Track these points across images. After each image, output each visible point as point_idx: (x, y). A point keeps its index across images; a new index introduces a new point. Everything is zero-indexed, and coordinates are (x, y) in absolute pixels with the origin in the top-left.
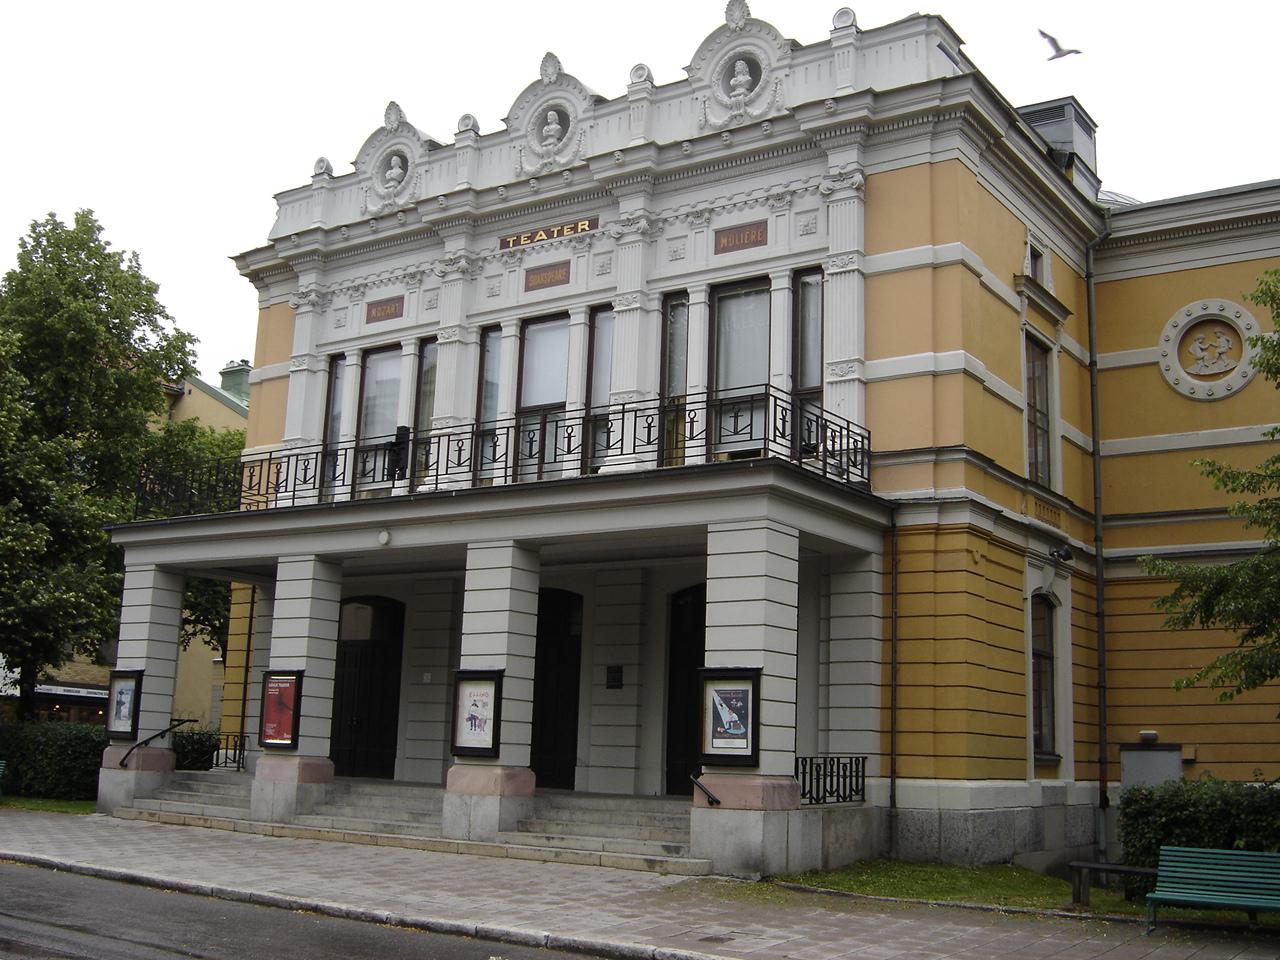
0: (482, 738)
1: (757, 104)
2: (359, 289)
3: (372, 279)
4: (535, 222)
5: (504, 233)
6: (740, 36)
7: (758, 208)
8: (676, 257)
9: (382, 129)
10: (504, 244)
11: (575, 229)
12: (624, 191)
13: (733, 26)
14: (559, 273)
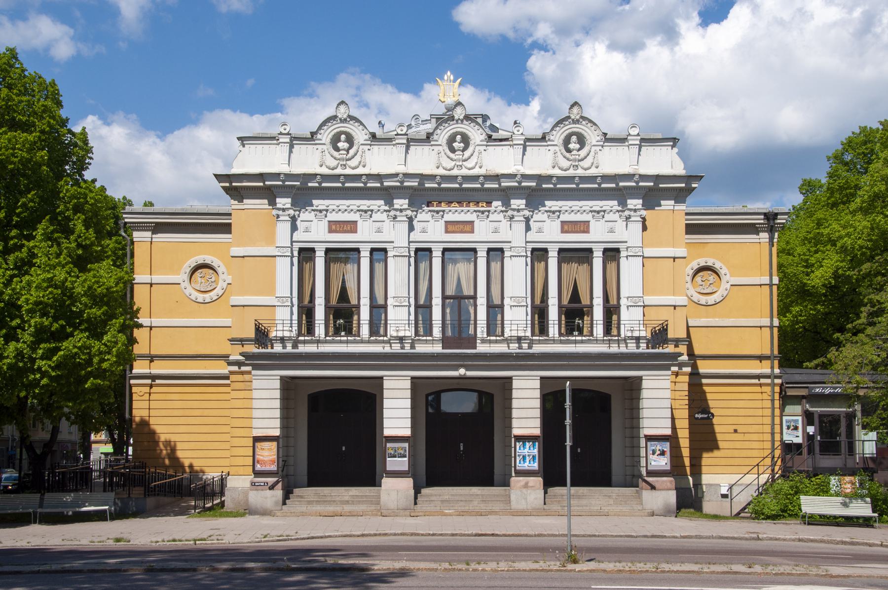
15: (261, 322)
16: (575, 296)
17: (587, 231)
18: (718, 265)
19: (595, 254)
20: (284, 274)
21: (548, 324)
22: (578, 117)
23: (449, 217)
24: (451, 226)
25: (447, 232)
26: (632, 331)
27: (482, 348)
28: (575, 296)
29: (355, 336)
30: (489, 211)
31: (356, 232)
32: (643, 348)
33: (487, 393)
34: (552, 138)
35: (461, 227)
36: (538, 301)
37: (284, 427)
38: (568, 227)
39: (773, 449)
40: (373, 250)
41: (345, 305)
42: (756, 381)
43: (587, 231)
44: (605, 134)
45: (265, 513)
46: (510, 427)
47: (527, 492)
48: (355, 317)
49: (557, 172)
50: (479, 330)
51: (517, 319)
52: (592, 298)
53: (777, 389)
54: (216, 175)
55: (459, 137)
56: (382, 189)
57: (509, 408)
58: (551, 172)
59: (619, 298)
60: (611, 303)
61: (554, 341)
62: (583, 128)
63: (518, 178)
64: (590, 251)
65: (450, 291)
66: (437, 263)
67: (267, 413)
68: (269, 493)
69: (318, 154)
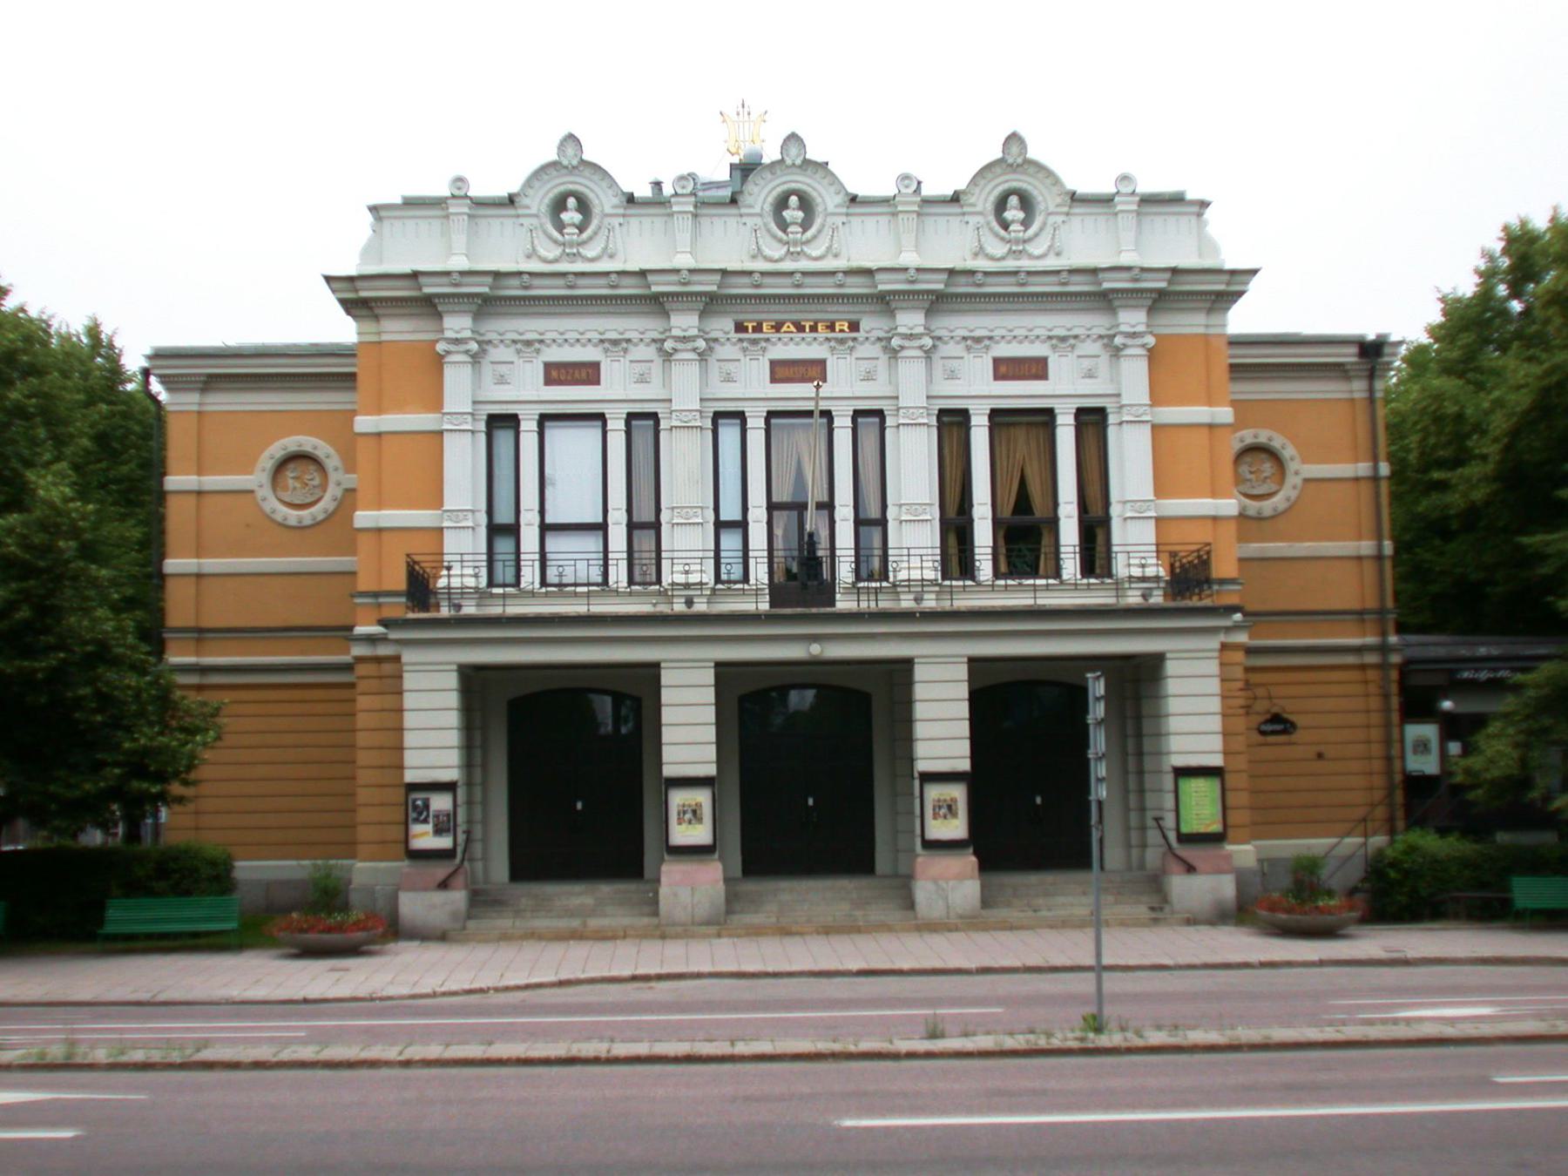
0: (1192, 787)
1: (592, 244)
2: (528, 345)
3: (549, 336)
4: (788, 314)
5: (741, 317)
6: (1014, 172)
7: (590, 348)
8: (501, 380)
9: (554, 164)
10: (740, 328)
11: (831, 327)
12: (450, 308)
13: (565, 162)
14: (814, 371)
15: (417, 558)
16: (1023, 503)
18: (1278, 442)
22: (575, 162)
24: (782, 371)
25: (774, 380)
26: (1143, 566)
27: (844, 603)
28: (1023, 503)
30: (855, 339)
31: (598, 383)
32: (1157, 599)
33: (630, 697)
34: (526, 201)
35: (802, 370)
36: (952, 513)
37: (468, 765)
39: (1390, 789)
40: (631, 417)
41: (1026, 518)
42: (1350, 659)
44: (1074, 194)
46: (911, 760)
47: (951, 883)
48: (1046, 540)
49: (982, 264)
51: (915, 544)
53: (1394, 675)
54: (328, 279)
55: (794, 200)
56: (648, 297)
57: (908, 721)
58: (971, 264)
59: (1107, 504)
60: (1092, 514)
64: (1049, 413)
65: (782, 495)
66: (529, 442)
68: (439, 897)
69: (970, 232)
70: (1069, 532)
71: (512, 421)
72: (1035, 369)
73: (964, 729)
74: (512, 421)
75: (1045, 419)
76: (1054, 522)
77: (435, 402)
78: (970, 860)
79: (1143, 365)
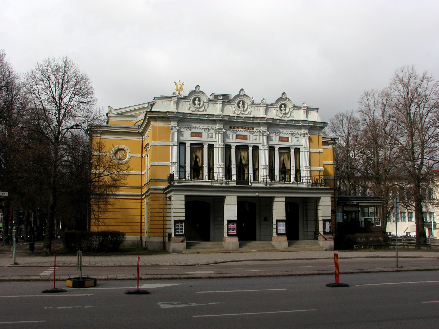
5: (231, 125)
14: (245, 137)
17: (288, 141)
19: (275, 149)
20: (173, 152)
21: (231, 175)
23: (239, 133)
25: (237, 138)
28: (196, 163)
29: (212, 179)
32: (310, 186)
35: (243, 137)
38: (193, 135)
43: (288, 141)
45: (180, 252)
47: (232, 242)
48: (201, 171)
50: (204, 176)
52: (185, 163)
61: (206, 181)
62: (286, 102)
63: (221, 116)
64: (247, 146)
67: (280, 211)
68: (182, 244)
70: (205, 170)
71: (184, 144)
72: (287, 139)
73: (184, 210)
74: (184, 144)
75: (201, 146)
76: (202, 167)
77: (168, 139)
78: (285, 238)
79: (176, 133)
